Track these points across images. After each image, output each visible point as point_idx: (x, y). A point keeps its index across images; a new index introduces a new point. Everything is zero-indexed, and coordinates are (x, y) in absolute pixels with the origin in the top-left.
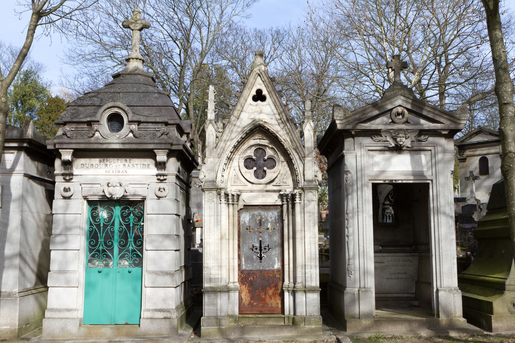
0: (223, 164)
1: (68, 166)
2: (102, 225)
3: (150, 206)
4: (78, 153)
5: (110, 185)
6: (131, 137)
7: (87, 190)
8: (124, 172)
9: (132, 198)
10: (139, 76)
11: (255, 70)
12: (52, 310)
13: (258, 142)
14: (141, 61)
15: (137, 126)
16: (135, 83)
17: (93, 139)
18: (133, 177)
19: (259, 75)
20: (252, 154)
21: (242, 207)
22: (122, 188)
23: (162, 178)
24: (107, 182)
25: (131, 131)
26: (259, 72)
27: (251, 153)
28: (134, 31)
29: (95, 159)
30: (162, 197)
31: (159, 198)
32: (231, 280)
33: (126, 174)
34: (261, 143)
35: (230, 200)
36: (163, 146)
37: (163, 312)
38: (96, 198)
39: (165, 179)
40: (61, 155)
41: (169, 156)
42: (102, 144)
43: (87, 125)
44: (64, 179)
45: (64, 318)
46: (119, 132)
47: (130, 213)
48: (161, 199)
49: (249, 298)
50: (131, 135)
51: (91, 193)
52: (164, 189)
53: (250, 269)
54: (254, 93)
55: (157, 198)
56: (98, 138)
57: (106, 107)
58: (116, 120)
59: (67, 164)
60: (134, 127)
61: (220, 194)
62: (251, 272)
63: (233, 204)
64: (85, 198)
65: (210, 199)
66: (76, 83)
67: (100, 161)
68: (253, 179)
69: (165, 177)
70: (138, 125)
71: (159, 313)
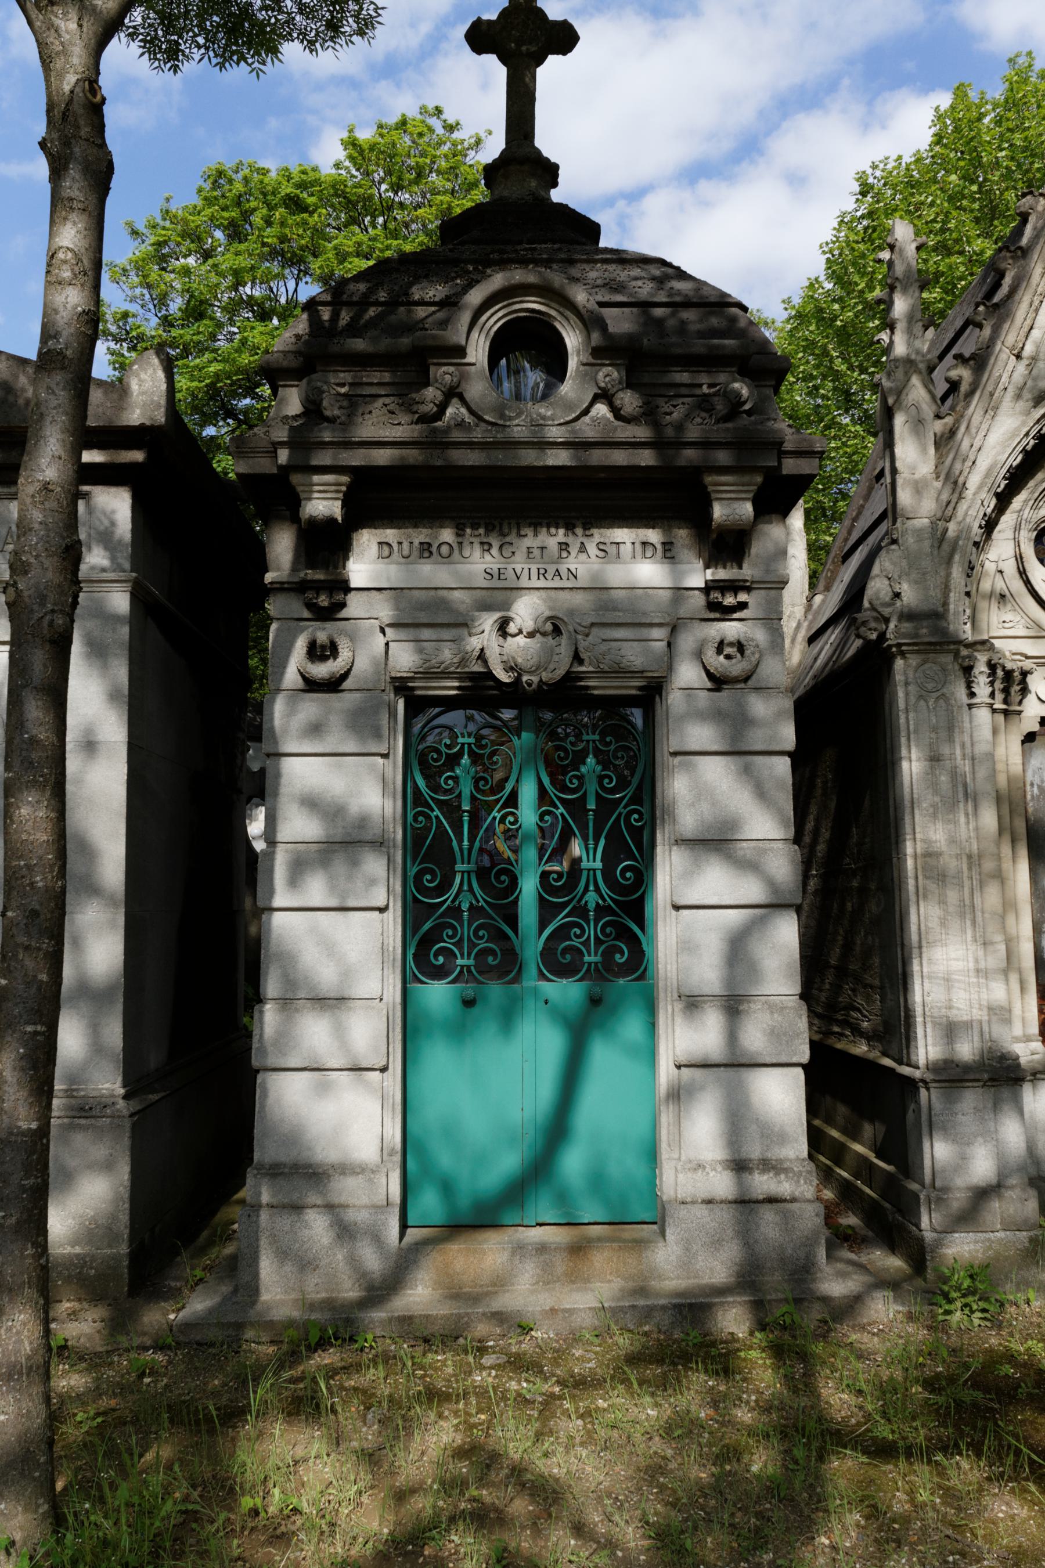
5: (512, 628)
6: (604, 417)
21: (1036, 727)
23: (729, 600)
39: (743, 606)
44: (310, 606)
65: (930, 686)
69: (743, 597)
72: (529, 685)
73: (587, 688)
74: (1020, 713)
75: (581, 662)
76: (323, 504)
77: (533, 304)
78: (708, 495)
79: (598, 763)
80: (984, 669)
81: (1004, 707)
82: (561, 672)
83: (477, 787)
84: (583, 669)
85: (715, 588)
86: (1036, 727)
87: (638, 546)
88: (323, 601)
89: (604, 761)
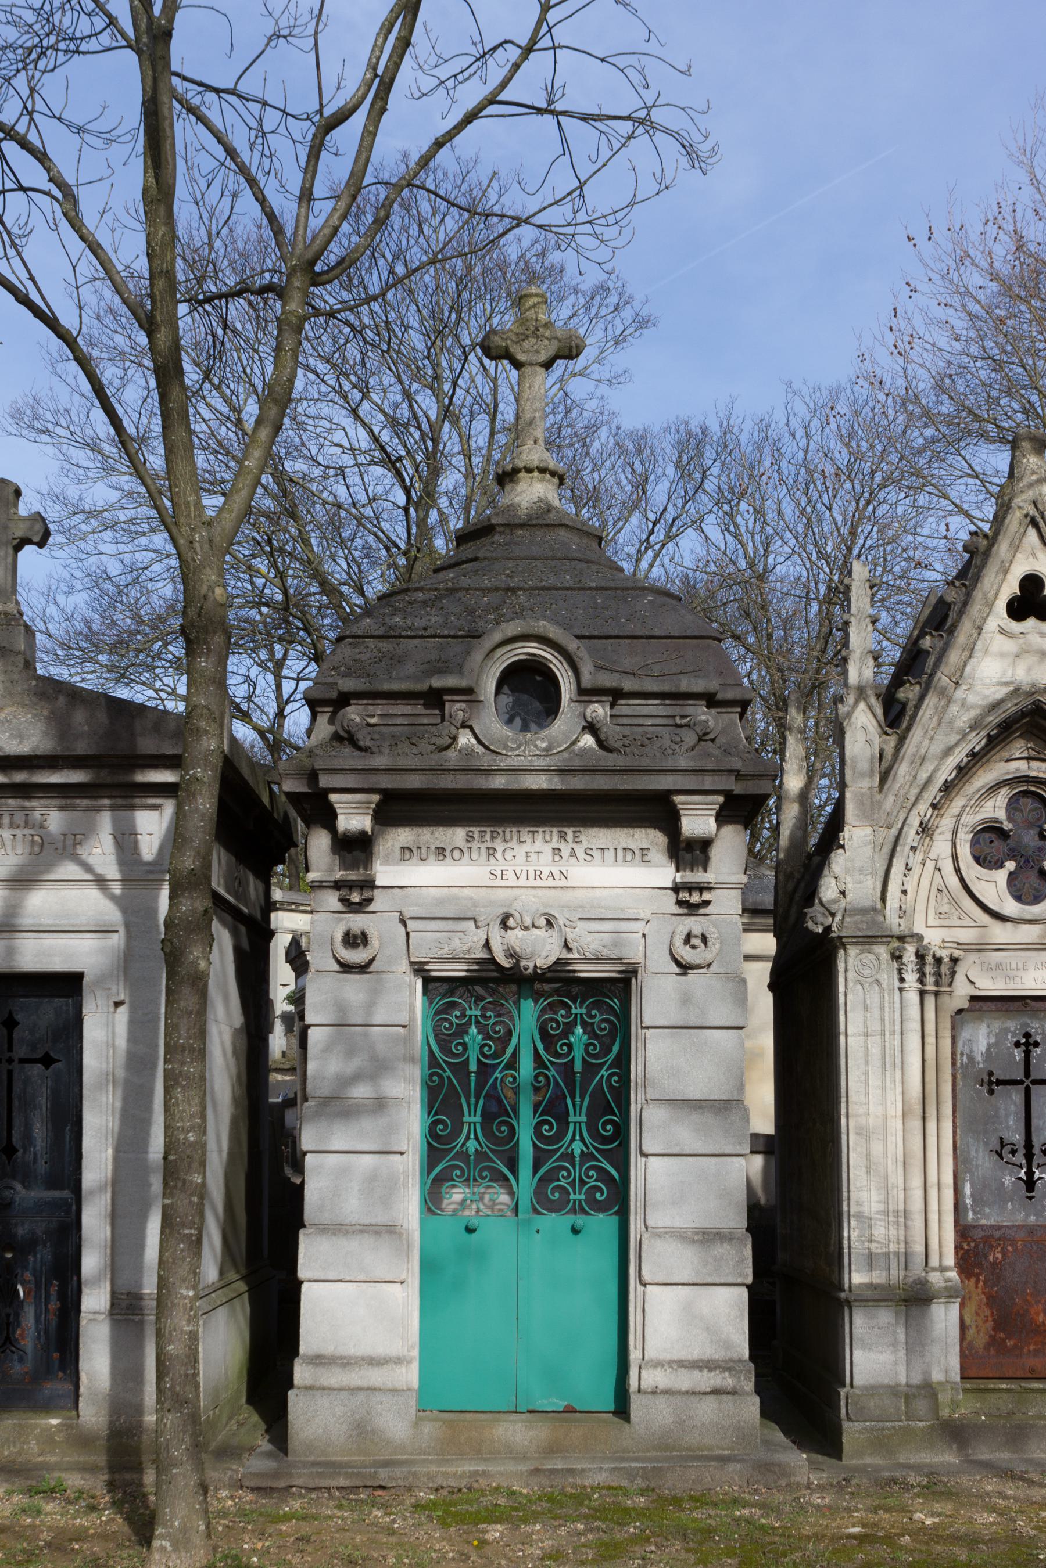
0: (907, 848)
1: (357, 853)
2: (473, 1067)
3: (657, 999)
4: (398, 808)
5: (511, 922)
6: (591, 748)
7: (434, 944)
8: (556, 874)
9: (587, 971)
10: (562, 533)
11: (1018, 501)
12: (319, 1360)
13: (1021, 767)
14: (556, 480)
15: (608, 708)
16: (554, 558)
17: (451, 754)
18: (591, 891)
19: (1034, 523)
20: (1001, 814)
21: (966, 1005)
22: (554, 932)
23: (695, 898)
24: (501, 911)
25: (591, 728)
26: (1032, 511)
27: (996, 808)
28: (528, 370)
29: (450, 831)
30: (699, 967)
31: (685, 968)
32: (934, 1262)
33: (563, 883)
34: (1033, 774)
35: (930, 980)
36: (708, 782)
37: (710, 1370)
38: (458, 970)
39: (707, 903)
40: (335, 816)
41: (723, 818)
42: (488, 772)
43: (426, 706)
45: (361, 1389)
46: (546, 732)
47: (574, 1024)
48: (692, 976)
49: (990, 1324)
50: (588, 740)
51: (444, 952)
52: (704, 939)
53: (992, 1222)
54: (1011, 587)
55: (677, 970)
56: (469, 753)
57: (498, 637)
58: (531, 690)
59: (355, 848)
60: (599, 710)
61: (900, 957)
62: (997, 1234)
63: (937, 994)
64: (419, 969)
66: (52, 610)
67: (470, 838)
68: (1011, 907)
69: (706, 896)
70: (612, 705)
71: (696, 1373)
72: (526, 969)
73: (575, 971)
74: (950, 993)
75: (570, 950)
76: (353, 817)
77: (533, 648)
78: (678, 811)
79: (584, 1033)
80: (913, 958)
81: (934, 988)
82: (552, 959)
83: (515, 1078)
84: (571, 956)
85: (684, 888)
86: (966, 1005)
87: (620, 853)
88: (355, 897)
89: (482, 1030)
